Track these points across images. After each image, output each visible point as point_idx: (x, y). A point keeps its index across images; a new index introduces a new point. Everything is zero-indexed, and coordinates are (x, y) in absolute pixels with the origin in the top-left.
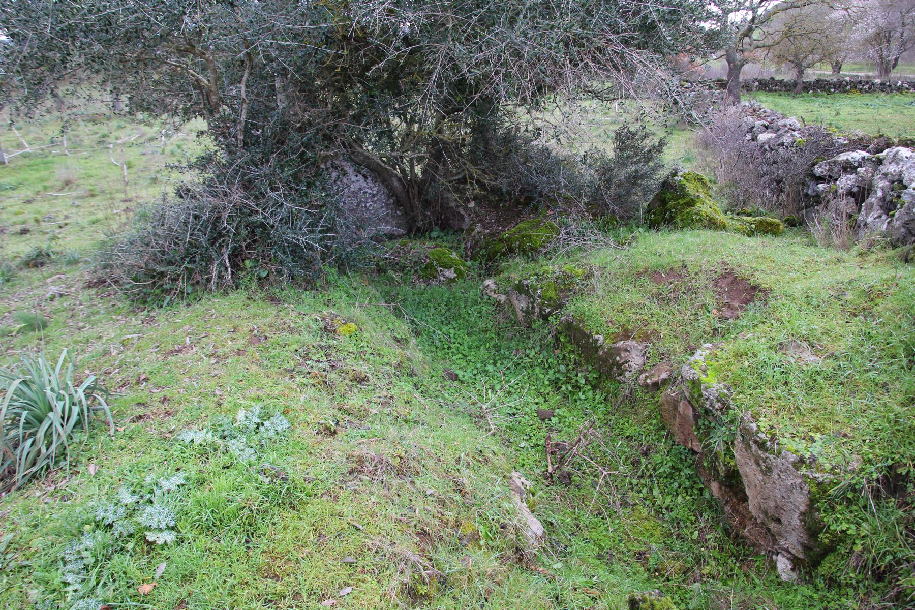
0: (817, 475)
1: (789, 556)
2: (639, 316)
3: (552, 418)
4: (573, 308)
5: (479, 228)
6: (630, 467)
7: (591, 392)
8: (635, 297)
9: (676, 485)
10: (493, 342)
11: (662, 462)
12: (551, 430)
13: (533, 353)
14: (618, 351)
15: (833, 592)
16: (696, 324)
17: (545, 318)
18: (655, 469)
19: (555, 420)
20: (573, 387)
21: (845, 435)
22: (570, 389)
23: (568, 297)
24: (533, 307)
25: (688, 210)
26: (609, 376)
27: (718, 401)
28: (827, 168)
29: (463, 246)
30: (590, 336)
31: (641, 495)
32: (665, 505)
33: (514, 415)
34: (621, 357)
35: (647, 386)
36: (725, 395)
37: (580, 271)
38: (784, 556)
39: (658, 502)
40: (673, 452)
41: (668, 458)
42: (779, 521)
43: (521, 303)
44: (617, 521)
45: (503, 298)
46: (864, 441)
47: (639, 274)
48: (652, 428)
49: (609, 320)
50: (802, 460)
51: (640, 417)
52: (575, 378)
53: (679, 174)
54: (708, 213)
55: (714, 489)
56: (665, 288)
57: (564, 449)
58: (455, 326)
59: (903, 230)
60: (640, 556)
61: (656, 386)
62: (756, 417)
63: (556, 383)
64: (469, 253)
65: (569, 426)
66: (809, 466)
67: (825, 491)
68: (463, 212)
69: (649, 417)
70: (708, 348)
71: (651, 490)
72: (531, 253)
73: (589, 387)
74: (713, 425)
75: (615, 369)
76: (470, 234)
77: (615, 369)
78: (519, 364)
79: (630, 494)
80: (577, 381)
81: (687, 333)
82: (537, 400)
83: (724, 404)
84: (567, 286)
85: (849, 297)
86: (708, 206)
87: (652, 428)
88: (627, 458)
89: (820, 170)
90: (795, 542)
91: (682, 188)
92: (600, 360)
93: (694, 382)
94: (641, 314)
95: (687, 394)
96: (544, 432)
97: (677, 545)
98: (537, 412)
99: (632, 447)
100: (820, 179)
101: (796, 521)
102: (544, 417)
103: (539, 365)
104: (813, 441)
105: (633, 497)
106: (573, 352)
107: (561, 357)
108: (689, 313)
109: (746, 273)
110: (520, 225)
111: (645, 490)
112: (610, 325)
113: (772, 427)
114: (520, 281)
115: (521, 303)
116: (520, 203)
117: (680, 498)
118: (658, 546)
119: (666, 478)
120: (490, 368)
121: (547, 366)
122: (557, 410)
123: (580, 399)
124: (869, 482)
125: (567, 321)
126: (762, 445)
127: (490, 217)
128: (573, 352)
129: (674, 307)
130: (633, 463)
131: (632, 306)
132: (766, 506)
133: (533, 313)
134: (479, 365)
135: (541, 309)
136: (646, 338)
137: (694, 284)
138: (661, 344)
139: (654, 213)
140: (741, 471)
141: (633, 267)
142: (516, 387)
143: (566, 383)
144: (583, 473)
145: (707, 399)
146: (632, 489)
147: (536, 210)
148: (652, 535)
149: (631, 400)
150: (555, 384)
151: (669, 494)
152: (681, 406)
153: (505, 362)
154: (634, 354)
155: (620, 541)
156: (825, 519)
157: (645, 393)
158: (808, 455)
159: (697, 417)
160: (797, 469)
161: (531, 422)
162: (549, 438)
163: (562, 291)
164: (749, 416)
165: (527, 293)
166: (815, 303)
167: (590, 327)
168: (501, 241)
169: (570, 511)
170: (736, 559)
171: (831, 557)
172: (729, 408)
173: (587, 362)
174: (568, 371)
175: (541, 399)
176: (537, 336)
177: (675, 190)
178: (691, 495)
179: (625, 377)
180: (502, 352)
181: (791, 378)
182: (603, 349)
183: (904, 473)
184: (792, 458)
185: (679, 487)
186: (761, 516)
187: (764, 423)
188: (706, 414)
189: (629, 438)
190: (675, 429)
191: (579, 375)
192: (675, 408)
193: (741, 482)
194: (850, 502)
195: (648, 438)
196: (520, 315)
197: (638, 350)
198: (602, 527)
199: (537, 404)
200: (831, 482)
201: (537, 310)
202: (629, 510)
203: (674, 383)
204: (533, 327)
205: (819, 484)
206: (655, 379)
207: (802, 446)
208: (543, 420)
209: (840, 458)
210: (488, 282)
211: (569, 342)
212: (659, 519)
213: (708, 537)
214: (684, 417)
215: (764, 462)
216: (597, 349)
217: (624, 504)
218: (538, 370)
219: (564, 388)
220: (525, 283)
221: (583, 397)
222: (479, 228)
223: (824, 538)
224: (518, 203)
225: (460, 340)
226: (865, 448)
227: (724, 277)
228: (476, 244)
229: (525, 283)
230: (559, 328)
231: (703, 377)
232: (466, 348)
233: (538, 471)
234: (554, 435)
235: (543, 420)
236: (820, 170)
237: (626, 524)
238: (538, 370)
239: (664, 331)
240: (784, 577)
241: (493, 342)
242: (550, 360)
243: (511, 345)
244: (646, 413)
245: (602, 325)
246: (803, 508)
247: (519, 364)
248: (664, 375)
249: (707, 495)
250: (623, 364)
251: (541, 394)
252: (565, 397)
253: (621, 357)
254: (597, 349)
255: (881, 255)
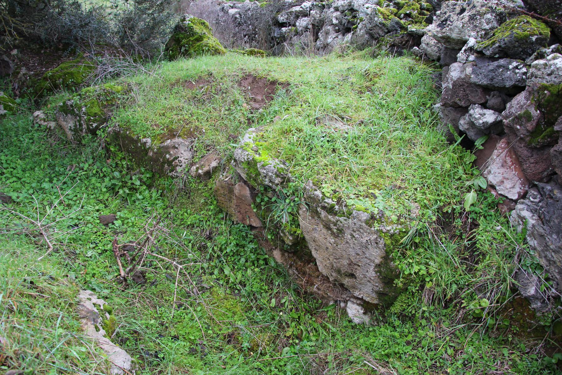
0: (388, 228)
1: (358, 302)
2: (180, 117)
3: (115, 222)
4: (119, 118)
5: (24, 70)
6: (198, 253)
7: (147, 191)
8: (173, 102)
9: (243, 260)
10: (47, 162)
11: (226, 243)
12: (116, 233)
13: (86, 166)
14: (167, 149)
15: (407, 326)
16: (232, 117)
17: (93, 132)
18: (221, 250)
19: (118, 223)
20: (130, 189)
21: (400, 188)
22: (127, 191)
23: (112, 111)
24: (81, 125)
25: (198, 44)
26: (162, 174)
27: (278, 176)
28: (286, 16)
29: (10, 88)
30: (138, 140)
31: (214, 277)
32: (238, 281)
33: (76, 225)
34: (170, 155)
35: (199, 176)
36: (282, 169)
37: (120, 88)
38: (353, 303)
39: (232, 280)
40: (234, 232)
41: (231, 237)
42: (352, 276)
43: (69, 124)
44: (199, 309)
45: (53, 124)
46: (416, 189)
47: (173, 85)
48: (210, 213)
49: (153, 123)
50: (373, 217)
51: (197, 205)
52: (130, 182)
53: (187, 19)
54: (214, 45)
55: (276, 257)
56: (199, 92)
57: (133, 249)
58: (7, 153)
59: (366, 36)
60: (230, 338)
61: (208, 175)
62: (318, 185)
63: (113, 189)
64: (17, 92)
65: (133, 226)
66: (380, 221)
67: (397, 241)
68: (6, 59)
69: (206, 204)
70: (253, 132)
71: (222, 270)
72: (74, 86)
73: (145, 187)
74: (273, 200)
75: (166, 166)
76: (16, 77)
77: (166, 166)
78: (75, 178)
79: (204, 278)
80: (133, 184)
81: (226, 126)
82: (97, 208)
83: (283, 178)
84: (109, 102)
85: (353, 79)
86: (212, 40)
87: (210, 213)
88: (193, 246)
89: (282, 18)
90: (370, 292)
91: (191, 29)
92: (151, 160)
93: (249, 163)
94: (182, 115)
95: (244, 176)
96: (110, 237)
97: (259, 316)
98: (100, 218)
99: (196, 234)
100: (283, 25)
101: (372, 273)
102: (106, 222)
103: (94, 175)
104: (376, 197)
105: (208, 281)
106: (124, 158)
107: (114, 165)
108: (223, 109)
109: (262, 74)
110: (61, 65)
111: (216, 271)
112: (155, 128)
113: (335, 192)
114: (64, 103)
115: (69, 124)
116: (59, 49)
117: (249, 272)
118: (243, 323)
119: (233, 256)
120: (46, 185)
121: (102, 175)
122: (118, 213)
123: (138, 199)
124: (430, 224)
125: (114, 131)
126: (330, 210)
127: (33, 61)
128: (124, 158)
129: (209, 107)
130: (199, 249)
131: (172, 109)
132: (339, 265)
133: (82, 131)
134: (34, 185)
135: (88, 125)
136: (190, 134)
137: (224, 87)
138: (204, 138)
139: (172, 50)
140: (307, 237)
141: (166, 80)
142: (75, 199)
143: (122, 187)
144: (156, 268)
145: (265, 177)
146: (204, 273)
147: (75, 53)
148: (234, 313)
149: (186, 192)
150: (112, 189)
151: (239, 269)
152: (237, 188)
153: (61, 178)
154: (182, 150)
155: (208, 328)
156: (400, 266)
157: (199, 183)
158: (376, 212)
159: (254, 195)
160: (370, 226)
161: (95, 230)
162: (116, 242)
163: (105, 107)
164: (311, 185)
165: (72, 113)
166: (329, 86)
167: (136, 132)
168: (46, 79)
169: (151, 311)
170: (311, 315)
171: (403, 297)
172: (289, 181)
173: (139, 166)
174: (123, 176)
175: (101, 206)
176: (88, 150)
177: (186, 31)
178: (257, 267)
179: (177, 172)
180: (57, 169)
181: (338, 145)
182: (153, 150)
183: (450, 211)
184: (365, 216)
185: (246, 261)
186: (334, 274)
187: (327, 188)
188: (262, 191)
189: (192, 226)
190: (232, 210)
191: (134, 178)
192: (231, 191)
193: (306, 247)
194: (417, 246)
195: (208, 223)
196: (70, 134)
197: (185, 145)
198: (187, 318)
199: (98, 211)
200: (401, 231)
201: (85, 126)
202: (208, 294)
203: (224, 169)
204: (83, 142)
205: (392, 236)
206: (206, 169)
207: (368, 203)
208: (107, 225)
209: (402, 207)
210: (37, 113)
211: (119, 150)
212: (235, 295)
213: (283, 301)
214: (240, 199)
215: (335, 225)
216: (146, 151)
217: (203, 289)
218: (93, 180)
219: (121, 192)
220: (69, 103)
221: (140, 197)
222: (24, 70)
223: (399, 283)
224: (58, 49)
225: (13, 165)
226: (419, 196)
227: (245, 79)
228: (23, 84)
229: (69, 103)
230: (108, 140)
231: (257, 157)
232: (20, 171)
233: (110, 277)
234: (120, 238)
235: (107, 225)
236: (282, 18)
237: (209, 310)
238: (93, 180)
239: (205, 126)
240: (356, 321)
241: (47, 162)
242: (104, 170)
243: (65, 162)
244: (202, 201)
245: (147, 129)
246: (377, 261)
247: (75, 178)
248: (214, 164)
249: (273, 264)
250: (174, 160)
251: (101, 201)
252: (124, 200)
253: (170, 155)
254: (146, 151)
255: (353, 55)
